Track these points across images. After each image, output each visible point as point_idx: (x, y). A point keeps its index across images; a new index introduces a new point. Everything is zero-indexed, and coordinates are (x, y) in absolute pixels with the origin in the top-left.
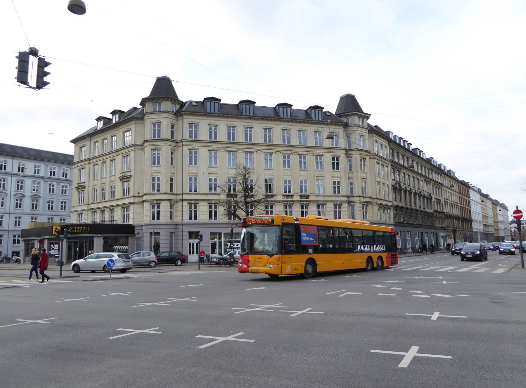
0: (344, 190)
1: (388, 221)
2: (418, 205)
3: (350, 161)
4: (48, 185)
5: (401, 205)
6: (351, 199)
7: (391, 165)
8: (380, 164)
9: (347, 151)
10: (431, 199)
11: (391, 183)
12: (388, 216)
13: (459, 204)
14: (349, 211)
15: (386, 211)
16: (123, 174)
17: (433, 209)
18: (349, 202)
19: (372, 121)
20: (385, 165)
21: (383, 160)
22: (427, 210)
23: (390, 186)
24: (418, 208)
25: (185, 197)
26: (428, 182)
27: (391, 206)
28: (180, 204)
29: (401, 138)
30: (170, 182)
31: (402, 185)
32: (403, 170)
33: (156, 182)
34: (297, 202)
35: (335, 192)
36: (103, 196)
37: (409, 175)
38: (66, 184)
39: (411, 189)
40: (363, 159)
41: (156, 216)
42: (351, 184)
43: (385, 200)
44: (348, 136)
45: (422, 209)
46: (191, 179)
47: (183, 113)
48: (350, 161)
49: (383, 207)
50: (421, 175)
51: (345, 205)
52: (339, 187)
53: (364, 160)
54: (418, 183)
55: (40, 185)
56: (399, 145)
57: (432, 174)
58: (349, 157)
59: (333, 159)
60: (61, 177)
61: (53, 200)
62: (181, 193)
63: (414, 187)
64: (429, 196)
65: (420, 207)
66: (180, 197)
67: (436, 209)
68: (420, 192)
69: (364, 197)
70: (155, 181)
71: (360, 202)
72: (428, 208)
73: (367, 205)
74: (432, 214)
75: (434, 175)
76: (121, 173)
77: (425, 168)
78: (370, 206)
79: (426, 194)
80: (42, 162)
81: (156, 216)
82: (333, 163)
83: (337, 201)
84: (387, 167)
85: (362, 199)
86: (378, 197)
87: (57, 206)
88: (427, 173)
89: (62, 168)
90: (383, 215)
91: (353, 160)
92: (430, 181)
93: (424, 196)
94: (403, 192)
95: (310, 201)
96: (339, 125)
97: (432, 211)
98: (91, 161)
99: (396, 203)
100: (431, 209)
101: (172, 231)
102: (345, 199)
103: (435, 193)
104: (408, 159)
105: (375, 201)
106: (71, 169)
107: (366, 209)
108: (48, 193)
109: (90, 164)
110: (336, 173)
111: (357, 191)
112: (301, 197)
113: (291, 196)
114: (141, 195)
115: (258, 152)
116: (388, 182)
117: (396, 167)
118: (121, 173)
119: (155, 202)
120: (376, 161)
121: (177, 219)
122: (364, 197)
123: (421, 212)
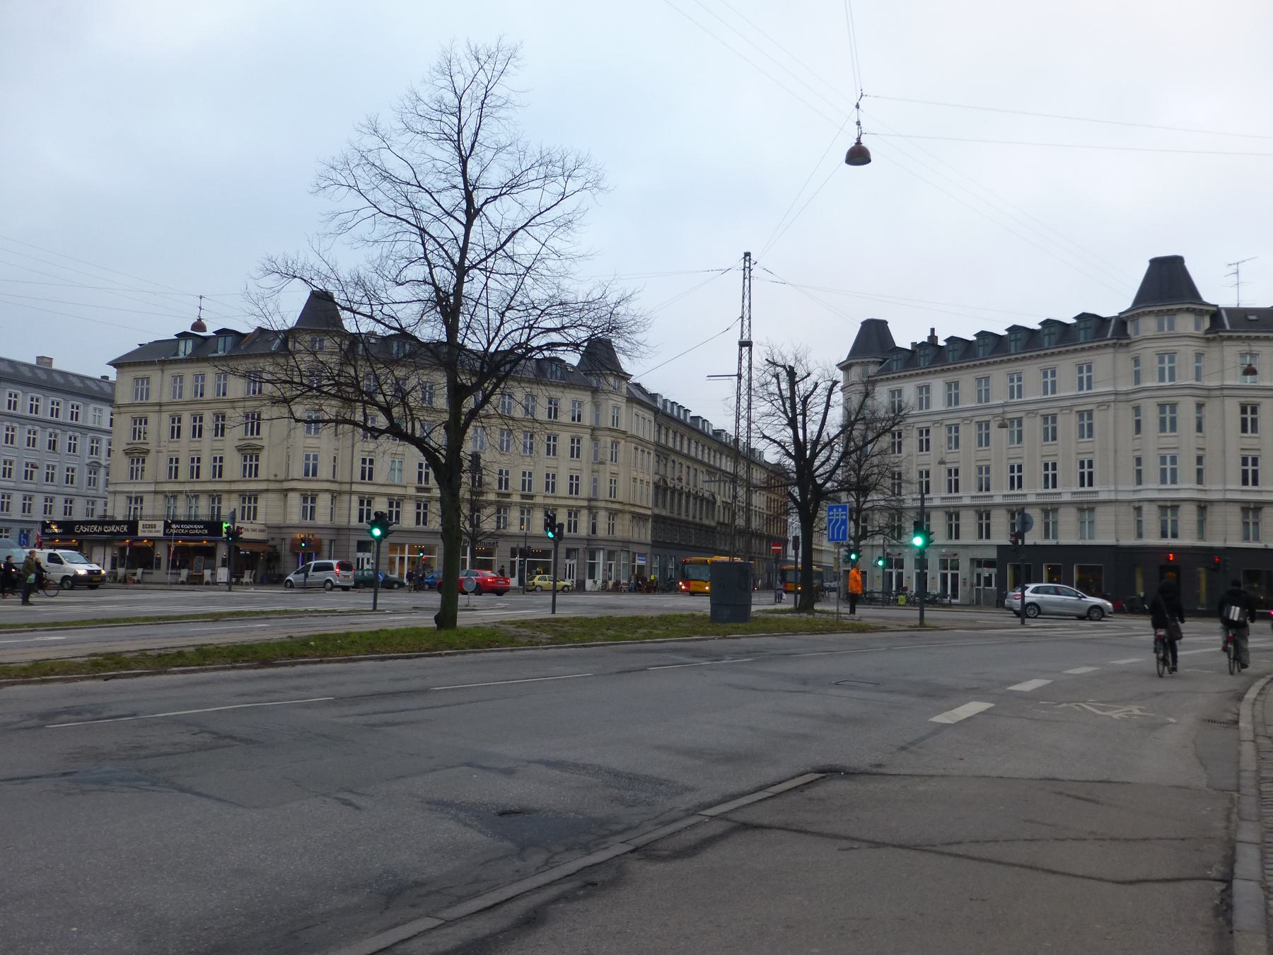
0: (585, 491)
1: (643, 539)
2: (690, 513)
3: (596, 445)
4: (5, 429)
5: (664, 513)
6: (594, 503)
7: (656, 450)
8: (639, 450)
9: (593, 429)
10: (714, 503)
11: (650, 477)
12: (643, 531)
13: (765, 511)
14: (589, 522)
15: (641, 523)
16: (245, 442)
17: (716, 518)
18: (590, 508)
19: (633, 380)
20: (646, 450)
21: (644, 443)
22: (706, 522)
23: (651, 484)
24: (691, 519)
25: (355, 488)
26: (712, 473)
27: (649, 516)
28: (346, 497)
29: (674, 402)
30: (332, 463)
31: (668, 481)
32: (673, 457)
33: (574, 482)
34: (516, 504)
35: (571, 492)
36: (196, 472)
37: (681, 464)
38: (77, 434)
39: (682, 488)
40: (615, 444)
41: (309, 512)
42: (595, 480)
43: (641, 507)
44: (597, 405)
45: (697, 520)
46: (364, 461)
47: (360, 357)
48: (596, 445)
49: (638, 518)
50: (701, 463)
51: (584, 513)
52: (577, 485)
53: (616, 446)
54: (696, 475)
55: (101, 445)
56: (671, 417)
57: (720, 459)
58: (594, 439)
59: (573, 441)
60: (28, 414)
61: (54, 464)
62: (348, 480)
63: (688, 484)
64: (711, 498)
65: (694, 517)
66: (346, 487)
67: (721, 520)
68: (697, 492)
69: (612, 502)
70: (309, 460)
71: (606, 509)
72: (707, 517)
73: (616, 514)
74: (715, 528)
75: (724, 461)
76: (128, 444)
77: (709, 449)
78: (620, 515)
79: (707, 494)
80: (60, 394)
81: (309, 512)
82: (572, 448)
83: (573, 506)
84: (649, 453)
85: (610, 505)
86: (632, 502)
87: (60, 475)
88: (712, 458)
89: (30, 394)
90: (636, 530)
91: (601, 443)
92: (715, 471)
93: (702, 499)
94: (669, 492)
95: (534, 504)
96: (586, 391)
97: (713, 524)
98: (163, 408)
99: (657, 511)
100: (713, 518)
101: (333, 537)
102: (585, 503)
103: (722, 493)
104: (682, 437)
105: (627, 508)
106: (86, 405)
107: (613, 520)
108: (67, 452)
109: (160, 411)
110: (575, 464)
111: (604, 492)
112: (523, 497)
113: (508, 495)
114: (278, 478)
115: (1101, 408)
116: (648, 477)
117: (663, 453)
118: (128, 444)
119: (309, 493)
120: (633, 445)
121: (341, 521)
122: (612, 502)
123: (696, 524)
